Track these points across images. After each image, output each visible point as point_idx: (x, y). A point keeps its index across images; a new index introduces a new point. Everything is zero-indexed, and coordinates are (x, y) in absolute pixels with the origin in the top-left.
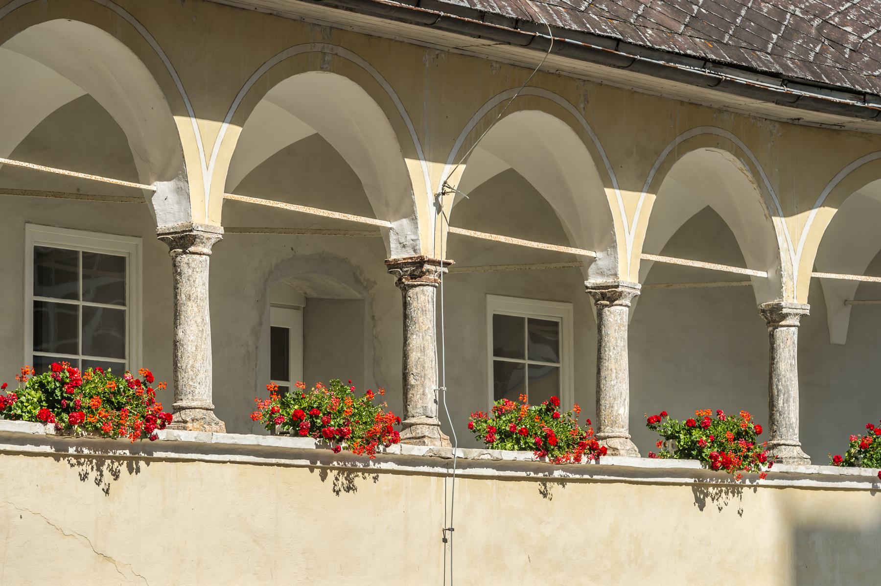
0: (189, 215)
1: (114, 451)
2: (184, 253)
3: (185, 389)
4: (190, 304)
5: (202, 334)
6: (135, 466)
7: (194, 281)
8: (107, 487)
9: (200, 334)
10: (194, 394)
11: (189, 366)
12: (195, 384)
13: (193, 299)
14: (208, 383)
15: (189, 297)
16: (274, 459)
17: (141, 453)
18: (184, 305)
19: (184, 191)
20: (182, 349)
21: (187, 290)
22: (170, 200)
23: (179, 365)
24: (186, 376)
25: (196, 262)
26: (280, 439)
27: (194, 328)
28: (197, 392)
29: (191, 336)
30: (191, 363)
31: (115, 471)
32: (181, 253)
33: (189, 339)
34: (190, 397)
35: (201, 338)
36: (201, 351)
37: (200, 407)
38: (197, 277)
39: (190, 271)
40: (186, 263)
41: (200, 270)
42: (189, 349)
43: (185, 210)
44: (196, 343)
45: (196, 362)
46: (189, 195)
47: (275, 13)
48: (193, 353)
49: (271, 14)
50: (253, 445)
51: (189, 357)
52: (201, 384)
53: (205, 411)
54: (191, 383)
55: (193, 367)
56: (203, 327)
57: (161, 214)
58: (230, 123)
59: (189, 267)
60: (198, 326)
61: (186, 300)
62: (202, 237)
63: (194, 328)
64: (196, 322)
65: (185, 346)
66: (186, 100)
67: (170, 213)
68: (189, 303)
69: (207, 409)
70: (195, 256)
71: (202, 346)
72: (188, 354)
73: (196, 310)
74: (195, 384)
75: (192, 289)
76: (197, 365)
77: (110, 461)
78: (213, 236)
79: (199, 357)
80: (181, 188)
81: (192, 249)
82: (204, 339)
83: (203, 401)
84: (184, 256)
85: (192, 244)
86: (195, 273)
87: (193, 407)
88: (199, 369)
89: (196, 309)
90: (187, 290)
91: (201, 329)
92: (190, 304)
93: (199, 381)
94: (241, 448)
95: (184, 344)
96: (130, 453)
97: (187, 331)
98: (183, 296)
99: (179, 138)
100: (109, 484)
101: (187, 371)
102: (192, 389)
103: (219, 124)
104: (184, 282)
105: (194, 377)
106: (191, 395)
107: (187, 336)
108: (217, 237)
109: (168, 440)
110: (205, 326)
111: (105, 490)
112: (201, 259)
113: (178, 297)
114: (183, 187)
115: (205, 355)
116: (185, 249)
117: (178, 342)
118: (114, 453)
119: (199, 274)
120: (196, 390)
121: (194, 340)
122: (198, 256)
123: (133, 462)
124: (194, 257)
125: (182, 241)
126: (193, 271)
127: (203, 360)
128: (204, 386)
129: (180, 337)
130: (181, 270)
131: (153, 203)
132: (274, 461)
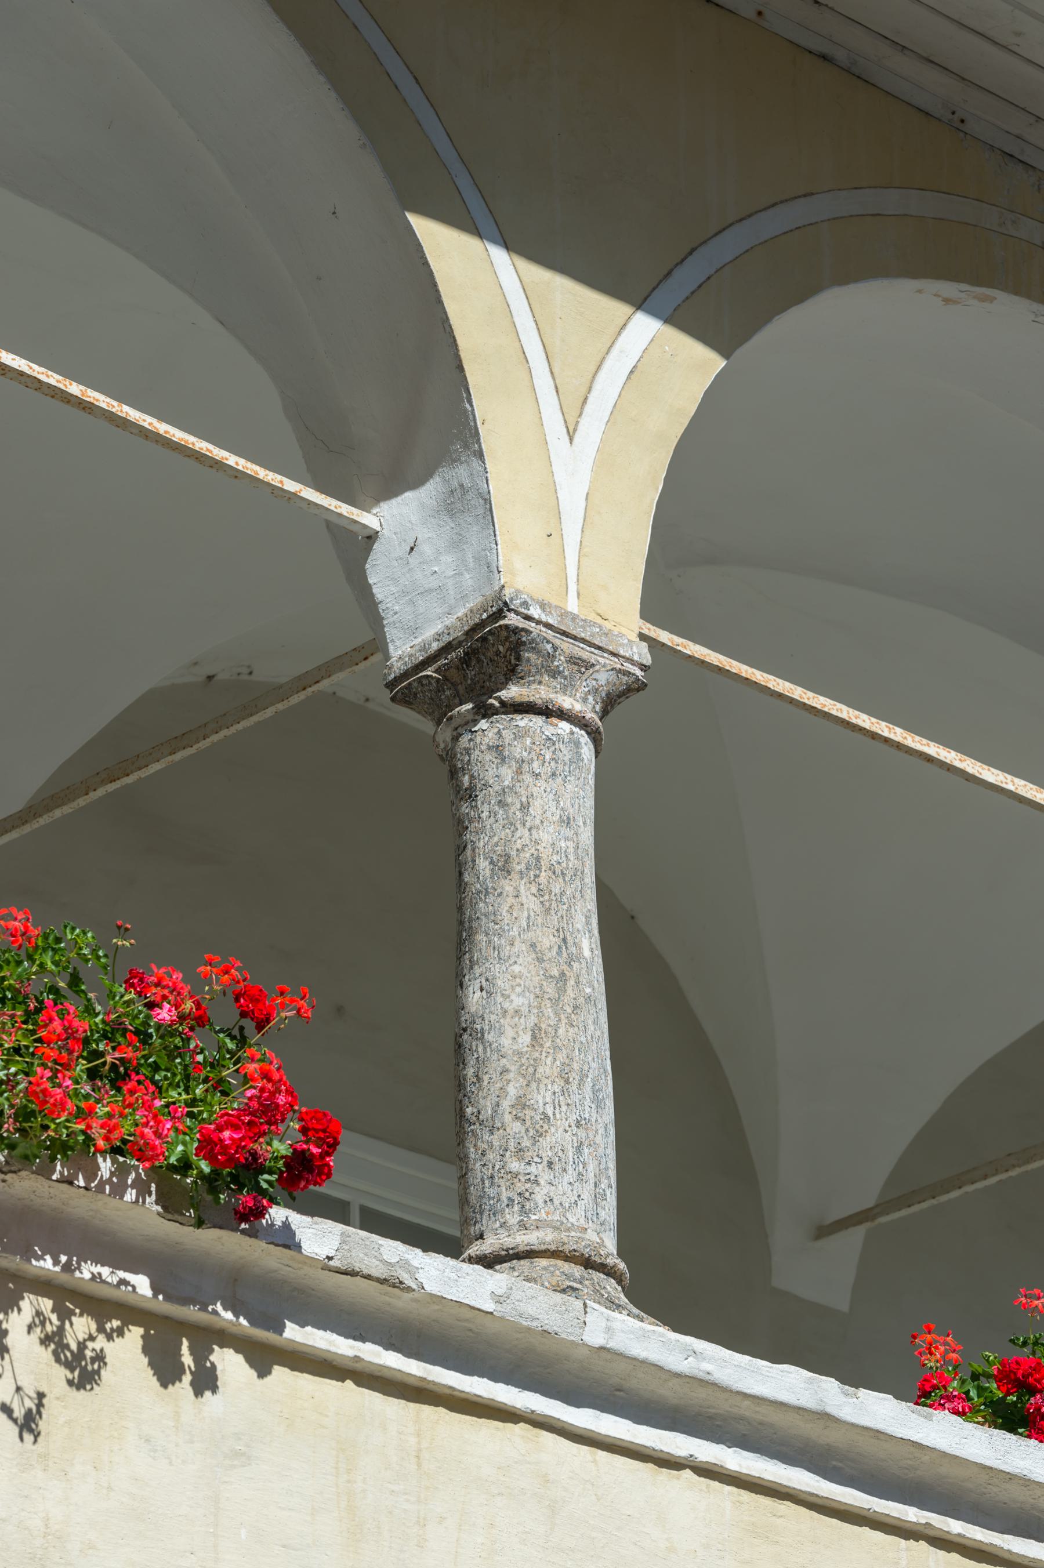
0: (490, 569)
1: (63, 1259)
2: (485, 712)
3: (491, 1192)
4: (507, 887)
5: (562, 990)
6: (187, 1359)
7: (525, 808)
8: (30, 1404)
9: (550, 990)
10: (528, 1205)
11: (506, 1104)
12: (532, 1169)
13: (522, 867)
14: (591, 1167)
15: (506, 862)
16: (915, 1509)
17: (219, 1307)
18: (487, 893)
19: (471, 495)
20: (480, 1048)
21: (496, 839)
22: (426, 549)
23: (469, 1110)
24: (496, 1143)
25: (528, 741)
26: (929, 1418)
27: (524, 966)
28: (539, 1198)
29: (513, 997)
30: (512, 1091)
31: (74, 1346)
32: (470, 717)
33: (506, 1005)
34: (512, 1218)
35: (556, 1002)
36: (556, 1048)
37: (553, 1247)
38: (535, 790)
39: (507, 774)
40: (489, 748)
41: (547, 769)
42: (506, 1042)
43: (476, 559)
44: (533, 1020)
45: (534, 1085)
46: (488, 501)
47: (840, 55)
48: (520, 1054)
49: (824, 57)
50: (799, 1410)
51: (507, 1071)
52: (557, 1166)
53: (577, 1271)
54: (515, 1165)
55: (521, 1103)
56: (565, 967)
57: (397, 608)
58: (673, 319)
59: (503, 759)
60: (540, 960)
61: (492, 877)
62: (549, 647)
63: (524, 966)
64: (533, 946)
65: (489, 1037)
66: (464, 182)
67: (430, 591)
68: (503, 882)
69: (588, 1263)
70: (523, 721)
71: (561, 1031)
72: (504, 1061)
73: (532, 906)
74: (532, 1169)
75: (518, 834)
76: (542, 1098)
77: (46, 1304)
78: (600, 660)
79: (548, 1068)
80: (462, 486)
81: (513, 692)
82: (569, 1010)
83: (568, 1230)
84: (483, 724)
85: (512, 673)
86: (528, 778)
87: (522, 1248)
88: (550, 1111)
89: (532, 903)
90: (496, 839)
91: (555, 972)
92: (507, 887)
93: (547, 1154)
94: (741, 1419)
95: (486, 1027)
96: (156, 1289)
97: (499, 982)
98: (483, 864)
99: (440, 302)
100: (41, 1396)
101: (498, 1124)
102: (520, 1187)
103: (619, 309)
104: (484, 815)
105: (526, 1143)
106: (516, 1208)
107: (499, 999)
108: (619, 666)
109: (353, 1273)
110: (575, 965)
111: (19, 1413)
112: (549, 731)
113: (467, 878)
114: (467, 483)
115: (576, 1066)
116: (484, 698)
117: (465, 1030)
118: (67, 1268)
119: (542, 783)
120: (537, 1189)
121: (524, 1010)
122: (538, 721)
123: (181, 1343)
124: (522, 724)
125: (471, 673)
126: (519, 772)
127: (567, 1082)
128: (571, 1175)
129: (473, 1009)
130: (472, 777)
131: (371, 581)
132: (912, 1514)
